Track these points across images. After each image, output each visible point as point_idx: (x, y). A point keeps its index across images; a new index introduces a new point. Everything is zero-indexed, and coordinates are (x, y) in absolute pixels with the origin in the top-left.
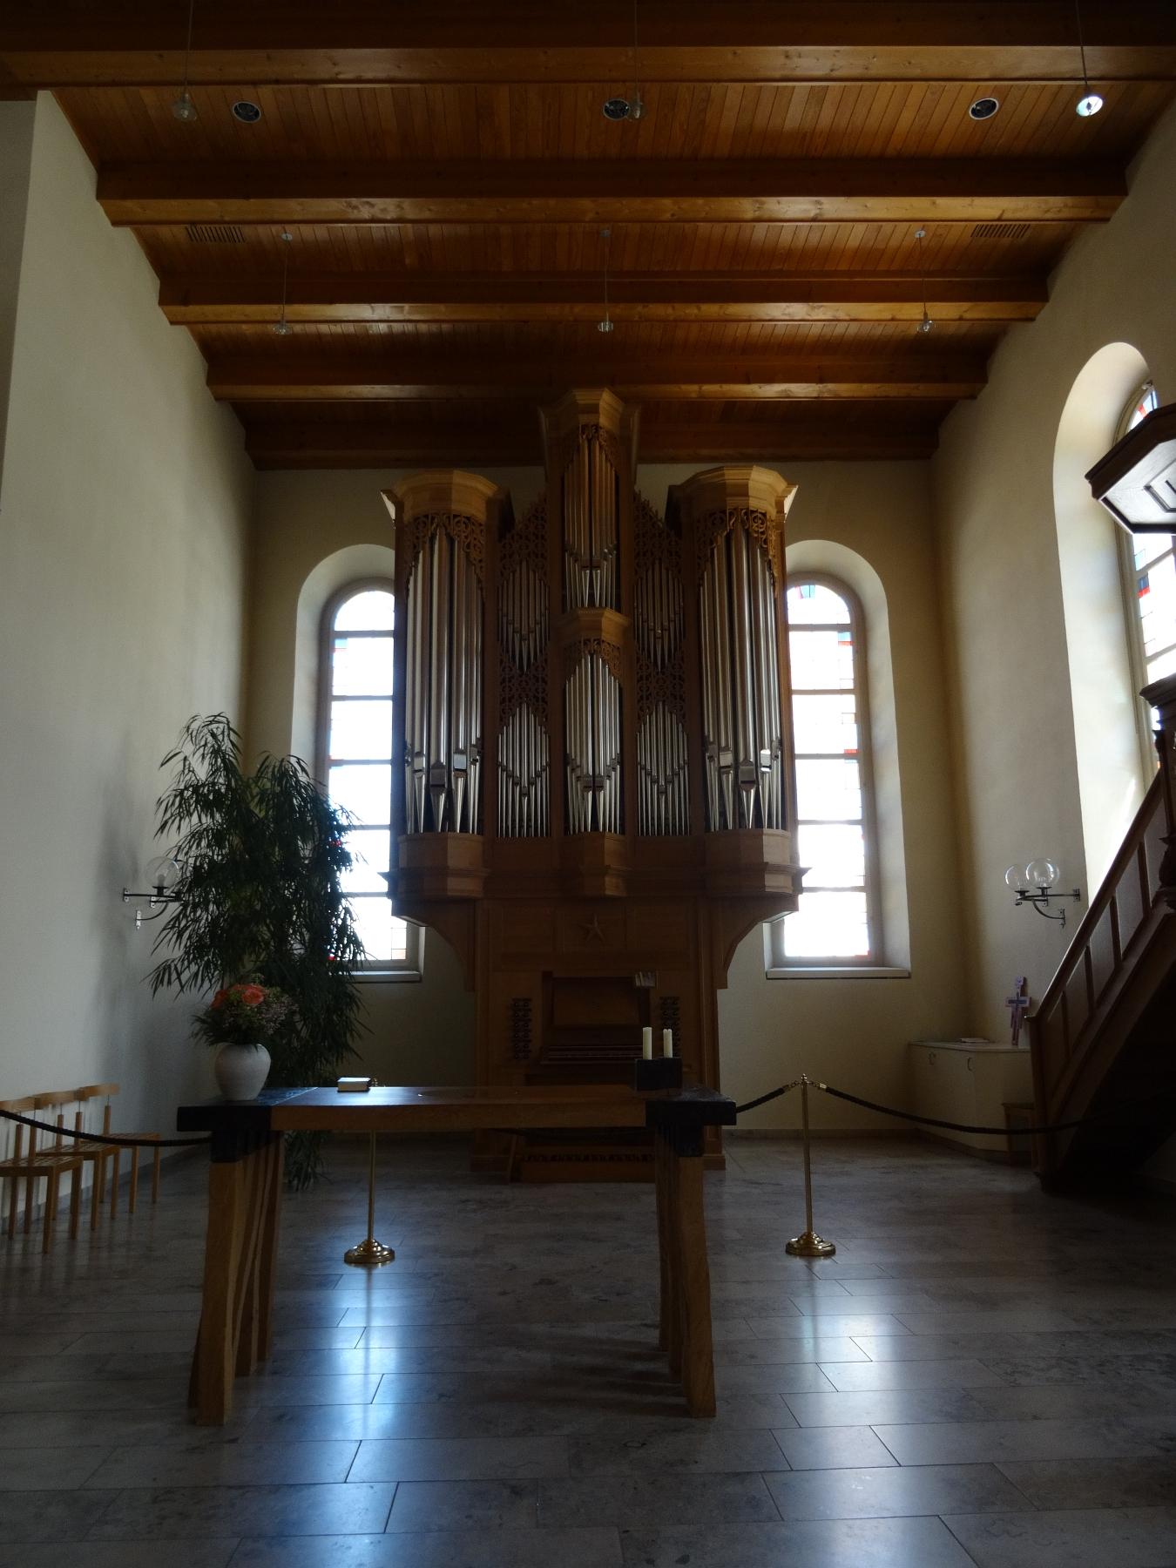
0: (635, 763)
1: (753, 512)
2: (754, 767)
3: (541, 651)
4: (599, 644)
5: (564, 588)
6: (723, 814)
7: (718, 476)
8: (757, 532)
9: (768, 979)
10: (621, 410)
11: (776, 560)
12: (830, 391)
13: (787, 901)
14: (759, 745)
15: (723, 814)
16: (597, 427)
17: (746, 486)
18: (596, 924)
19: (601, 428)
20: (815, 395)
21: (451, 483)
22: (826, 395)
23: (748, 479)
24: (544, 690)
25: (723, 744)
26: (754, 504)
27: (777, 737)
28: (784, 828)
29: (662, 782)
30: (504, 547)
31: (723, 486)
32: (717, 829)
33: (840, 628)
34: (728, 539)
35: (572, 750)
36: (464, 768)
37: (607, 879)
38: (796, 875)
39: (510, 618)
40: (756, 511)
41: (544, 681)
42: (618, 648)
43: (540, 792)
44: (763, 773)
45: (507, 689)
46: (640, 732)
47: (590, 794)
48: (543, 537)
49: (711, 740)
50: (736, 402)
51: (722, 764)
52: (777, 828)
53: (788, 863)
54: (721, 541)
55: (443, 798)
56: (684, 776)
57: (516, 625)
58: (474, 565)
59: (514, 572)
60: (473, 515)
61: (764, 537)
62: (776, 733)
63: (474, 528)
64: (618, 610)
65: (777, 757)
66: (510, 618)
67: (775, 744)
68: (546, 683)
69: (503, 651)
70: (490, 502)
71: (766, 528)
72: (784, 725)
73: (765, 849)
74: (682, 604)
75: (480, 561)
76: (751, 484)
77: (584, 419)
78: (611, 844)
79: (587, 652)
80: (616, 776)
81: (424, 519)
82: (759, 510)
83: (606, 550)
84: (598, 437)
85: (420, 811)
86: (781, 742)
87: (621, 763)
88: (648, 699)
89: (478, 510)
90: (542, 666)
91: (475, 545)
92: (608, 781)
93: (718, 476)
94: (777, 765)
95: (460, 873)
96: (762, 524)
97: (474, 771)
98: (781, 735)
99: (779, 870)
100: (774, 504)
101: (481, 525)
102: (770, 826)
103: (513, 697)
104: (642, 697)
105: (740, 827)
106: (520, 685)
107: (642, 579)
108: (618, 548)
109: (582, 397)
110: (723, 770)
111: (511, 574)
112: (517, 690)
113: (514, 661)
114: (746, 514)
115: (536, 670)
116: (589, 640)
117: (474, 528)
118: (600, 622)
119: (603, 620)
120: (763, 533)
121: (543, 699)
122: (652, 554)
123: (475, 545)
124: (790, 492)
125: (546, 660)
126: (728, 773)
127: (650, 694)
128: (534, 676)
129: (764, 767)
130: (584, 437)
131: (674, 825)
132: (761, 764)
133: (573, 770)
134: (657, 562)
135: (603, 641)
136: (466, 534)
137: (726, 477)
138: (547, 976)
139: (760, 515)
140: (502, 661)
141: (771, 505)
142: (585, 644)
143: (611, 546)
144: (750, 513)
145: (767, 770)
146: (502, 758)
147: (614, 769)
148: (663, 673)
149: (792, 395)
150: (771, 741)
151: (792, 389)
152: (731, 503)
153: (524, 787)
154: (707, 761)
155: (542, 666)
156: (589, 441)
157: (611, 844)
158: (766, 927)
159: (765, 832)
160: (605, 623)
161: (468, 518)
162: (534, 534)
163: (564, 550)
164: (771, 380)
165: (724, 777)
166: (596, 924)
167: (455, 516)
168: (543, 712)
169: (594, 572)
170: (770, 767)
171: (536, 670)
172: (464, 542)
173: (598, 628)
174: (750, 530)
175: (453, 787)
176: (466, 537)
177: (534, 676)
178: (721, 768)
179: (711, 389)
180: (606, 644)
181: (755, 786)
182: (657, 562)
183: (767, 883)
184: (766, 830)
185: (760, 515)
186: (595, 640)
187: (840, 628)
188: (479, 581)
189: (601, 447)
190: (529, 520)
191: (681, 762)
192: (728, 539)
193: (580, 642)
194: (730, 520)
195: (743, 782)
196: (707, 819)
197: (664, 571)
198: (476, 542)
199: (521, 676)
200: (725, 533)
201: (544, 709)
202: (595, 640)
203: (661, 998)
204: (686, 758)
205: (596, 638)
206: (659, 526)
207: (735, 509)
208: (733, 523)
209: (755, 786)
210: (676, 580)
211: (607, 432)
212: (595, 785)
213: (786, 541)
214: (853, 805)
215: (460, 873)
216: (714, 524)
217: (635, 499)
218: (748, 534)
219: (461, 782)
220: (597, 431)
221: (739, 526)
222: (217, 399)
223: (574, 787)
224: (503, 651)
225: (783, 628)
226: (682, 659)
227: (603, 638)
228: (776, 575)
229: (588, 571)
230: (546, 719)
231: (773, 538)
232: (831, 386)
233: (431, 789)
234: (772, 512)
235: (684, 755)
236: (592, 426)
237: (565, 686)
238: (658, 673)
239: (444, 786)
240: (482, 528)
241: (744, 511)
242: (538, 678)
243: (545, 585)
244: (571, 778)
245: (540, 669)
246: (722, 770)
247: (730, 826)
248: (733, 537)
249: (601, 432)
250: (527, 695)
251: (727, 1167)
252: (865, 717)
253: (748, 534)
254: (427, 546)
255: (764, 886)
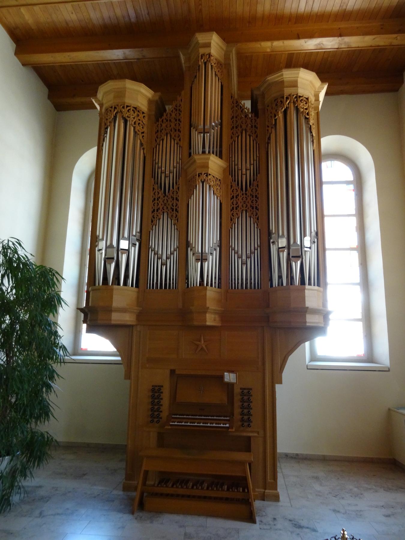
0: (229, 246)
1: (300, 97)
2: (300, 247)
3: (176, 183)
4: (207, 176)
5: (190, 148)
6: (280, 277)
7: (279, 77)
8: (303, 108)
9: (307, 369)
10: (225, 48)
11: (314, 126)
12: (345, 43)
13: (319, 330)
14: (303, 234)
15: (280, 277)
16: (210, 55)
17: (296, 82)
18: (203, 342)
19: (212, 56)
20: (336, 47)
21: (125, 88)
22: (343, 46)
23: (298, 77)
24: (177, 204)
25: (281, 233)
26: (301, 91)
27: (314, 231)
28: (318, 285)
29: (244, 257)
30: (157, 126)
31: (283, 82)
32: (277, 285)
33: (348, 183)
34: (285, 113)
35: (191, 239)
36: (127, 248)
37: (208, 315)
38: (325, 315)
39: (160, 165)
40: (302, 96)
41: (177, 200)
42: (220, 180)
43: (172, 264)
44: (306, 251)
45: (156, 204)
46: (232, 229)
47: (199, 264)
48: (179, 120)
49: (274, 232)
50: (294, 53)
51: (280, 246)
52: (314, 285)
53: (321, 308)
54: (281, 115)
55: (299, 263)
56: (257, 253)
57: (163, 169)
58: (139, 134)
59: (163, 140)
60: (138, 106)
61: (307, 111)
62: (314, 228)
63: (139, 113)
64: (221, 157)
65: (314, 242)
66: (160, 165)
67: (313, 234)
68: (178, 201)
69: (155, 183)
70: (150, 102)
71: (308, 106)
72: (318, 207)
73: (307, 299)
74: (258, 155)
75: (143, 133)
76: (299, 80)
77: (202, 51)
78: (211, 293)
79: (199, 181)
80: (216, 254)
81: (111, 109)
82: (304, 96)
83: (213, 124)
84: (210, 61)
85: (100, 275)
86: (317, 234)
87: (220, 246)
88: (236, 209)
89: (143, 104)
90: (176, 191)
91: (139, 124)
92: (211, 256)
93: (279, 77)
94: (314, 247)
95: (123, 310)
96: (306, 103)
97: (134, 252)
98: (317, 229)
99: (315, 312)
100: (313, 95)
101: (143, 113)
102: (310, 284)
103: (159, 209)
104: (233, 208)
105: (291, 284)
106: (163, 202)
107: (235, 141)
108: (221, 124)
109: (201, 38)
110: (280, 249)
111: (161, 141)
112: (162, 205)
113: (161, 189)
114: (296, 97)
115: (173, 193)
116: (201, 174)
117: (139, 113)
118: (208, 163)
119: (210, 162)
120: (306, 109)
121: (176, 210)
122: (241, 127)
123: (139, 124)
124: (323, 88)
125: (178, 188)
126: (283, 251)
127: (238, 206)
128: (172, 197)
129: (306, 247)
130: (202, 61)
131: (251, 283)
132: (304, 246)
133: (191, 250)
134: (244, 132)
135: (210, 175)
136: (133, 117)
137: (284, 76)
138: (172, 372)
139: (304, 99)
140: (154, 189)
141: (312, 94)
142: (199, 176)
143: (217, 122)
144: (298, 97)
145: (308, 249)
146: (152, 243)
147: (215, 249)
148: (246, 194)
149: (323, 47)
150: (311, 232)
151: (324, 43)
152: (287, 91)
153: (164, 260)
154: (271, 244)
155: (176, 191)
156: (205, 64)
157: (211, 293)
158: (307, 344)
159: (306, 288)
160: (211, 164)
161: (136, 108)
162: (174, 118)
163: (191, 126)
164: (311, 36)
165: (281, 254)
166: (203, 342)
167: (127, 106)
168: (176, 217)
169: (205, 135)
170: (310, 248)
171: (173, 193)
172: (132, 121)
173: (206, 166)
174: (299, 107)
175: (120, 259)
176: (134, 118)
177: (172, 197)
178: (279, 248)
179: (278, 44)
180: (210, 176)
181: (301, 259)
182: (244, 132)
183: (307, 320)
184: (307, 286)
185: (304, 99)
186: (204, 174)
187: (348, 183)
188: (142, 144)
189: (212, 66)
190: (172, 111)
191: (256, 246)
192: (285, 113)
193: (196, 175)
194: (286, 101)
195: (292, 257)
196: (271, 280)
197: (248, 137)
198: (140, 122)
199: (164, 197)
200: (283, 109)
201: (176, 215)
202: (204, 174)
203: (241, 389)
204: (259, 243)
205: (205, 173)
206: (245, 111)
207: (290, 95)
208: (288, 104)
209: (301, 259)
210: (255, 142)
211: (216, 59)
212: (203, 259)
213: (321, 135)
214: (356, 275)
215: (123, 310)
216: (276, 105)
217: (232, 97)
218: (297, 109)
219: (124, 257)
220: (209, 57)
221: (292, 104)
222: (24, 65)
223: (191, 258)
224: (155, 183)
225: (319, 183)
226: (258, 185)
227: (209, 173)
228: (314, 135)
229: (202, 135)
230: (178, 221)
231: (313, 114)
232: (347, 39)
233: (106, 260)
234: (312, 99)
235: (257, 242)
236: (207, 55)
237: (189, 202)
238: (243, 194)
239: (113, 258)
240: (144, 115)
241: (295, 96)
242: (174, 198)
243: (180, 147)
244: (190, 253)
245: (175, 193)
246: (280, 250)
247: (285, 284)
248: (288, 112)
249: (212, 58)
250: (167, 208)
251: (281, 490)
252: (362, 229)
253: (297, 109)
254: (113, 124)
255: (306, 322)
